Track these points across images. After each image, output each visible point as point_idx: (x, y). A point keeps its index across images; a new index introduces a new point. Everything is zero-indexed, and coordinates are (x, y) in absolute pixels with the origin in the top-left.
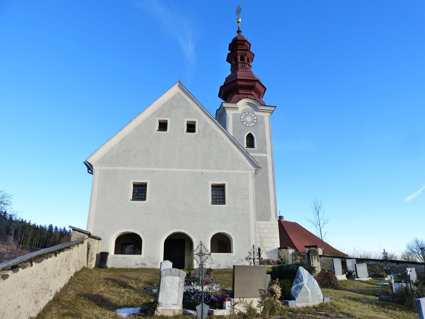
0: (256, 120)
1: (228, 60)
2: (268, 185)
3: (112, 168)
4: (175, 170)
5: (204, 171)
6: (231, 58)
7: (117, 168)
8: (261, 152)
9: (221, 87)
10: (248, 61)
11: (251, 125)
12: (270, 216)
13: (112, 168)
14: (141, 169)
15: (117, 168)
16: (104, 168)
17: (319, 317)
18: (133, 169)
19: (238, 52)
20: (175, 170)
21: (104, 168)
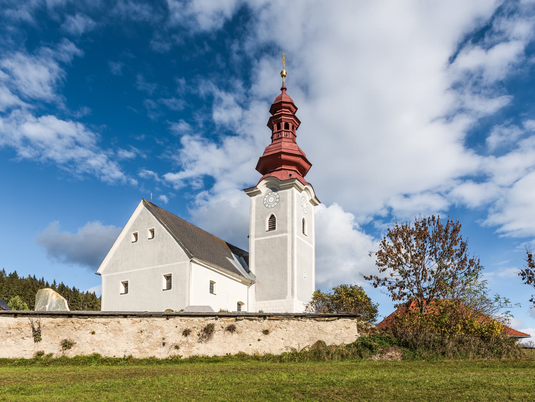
0: (279, 198)
1: (270, 125)
2: (286, 264)
3: (110, 274)
4: (143, 269)
5: (159, 266)
6: (274, 123)
7: (113, 274)
8: (282, 232)
9: (260, 158)
10: (293, 129)
11: (273, 206)
12: (286, 294)
13: (110, 274)
14: (124, 272)
15: (113, 274)
16: (107, 275)
17: (56, 397)
18: (120, 273)
19: (283, 117)
20: (143, 269)
21: (107, 275)
